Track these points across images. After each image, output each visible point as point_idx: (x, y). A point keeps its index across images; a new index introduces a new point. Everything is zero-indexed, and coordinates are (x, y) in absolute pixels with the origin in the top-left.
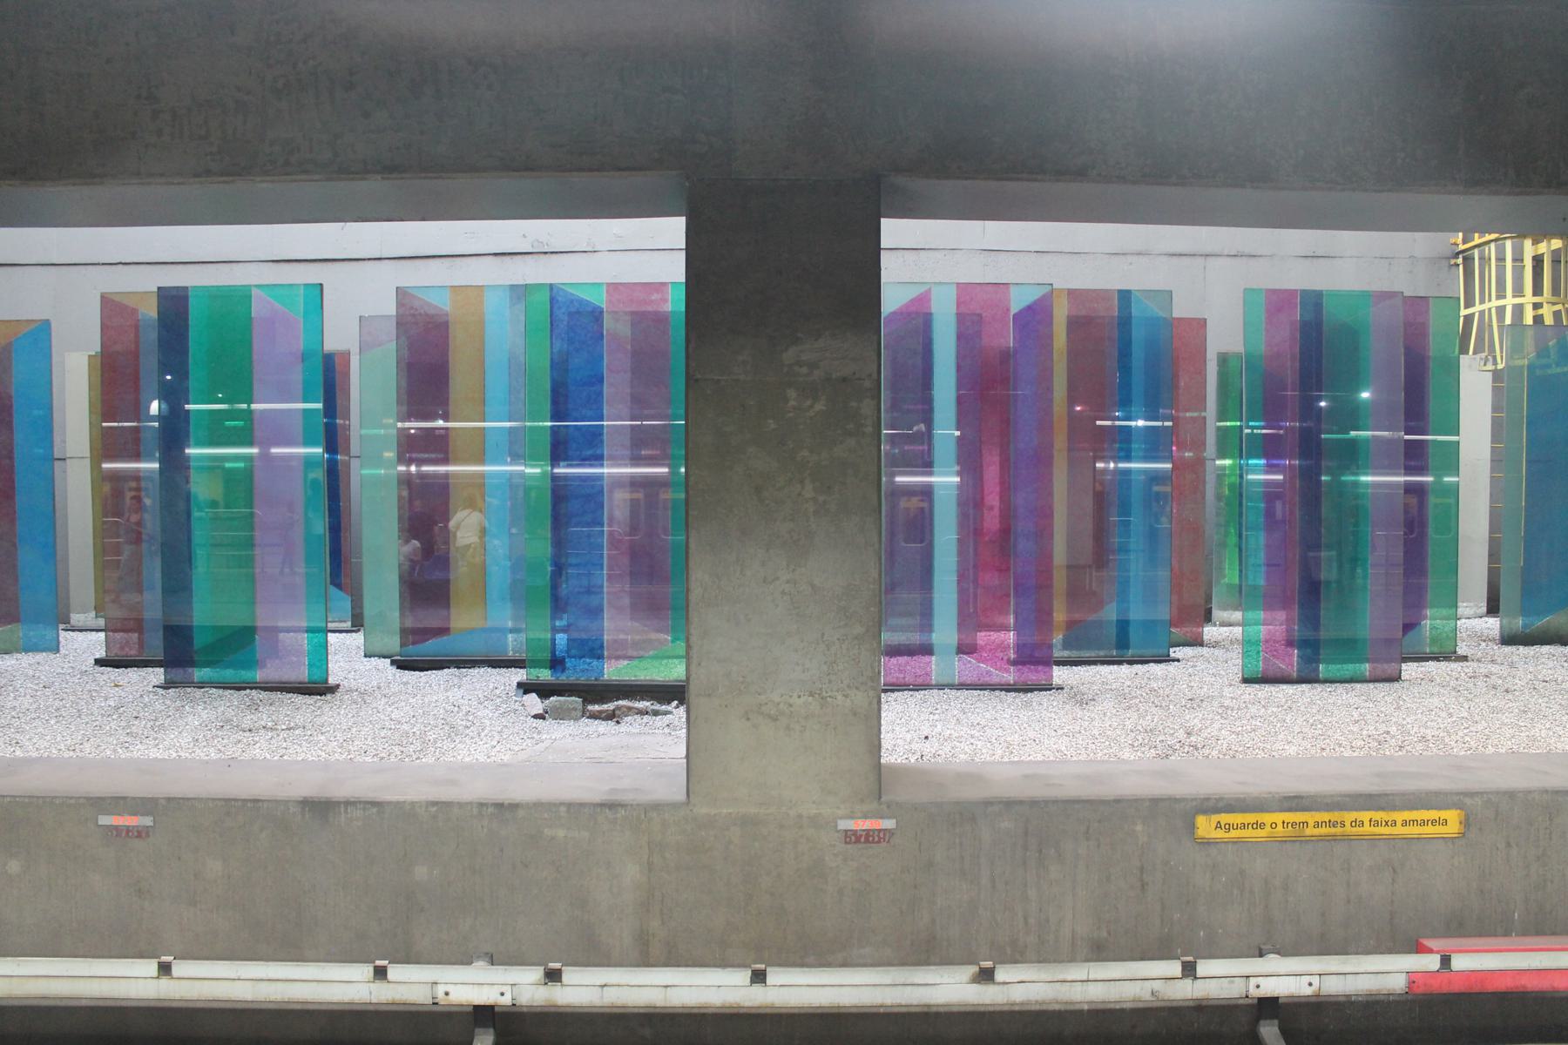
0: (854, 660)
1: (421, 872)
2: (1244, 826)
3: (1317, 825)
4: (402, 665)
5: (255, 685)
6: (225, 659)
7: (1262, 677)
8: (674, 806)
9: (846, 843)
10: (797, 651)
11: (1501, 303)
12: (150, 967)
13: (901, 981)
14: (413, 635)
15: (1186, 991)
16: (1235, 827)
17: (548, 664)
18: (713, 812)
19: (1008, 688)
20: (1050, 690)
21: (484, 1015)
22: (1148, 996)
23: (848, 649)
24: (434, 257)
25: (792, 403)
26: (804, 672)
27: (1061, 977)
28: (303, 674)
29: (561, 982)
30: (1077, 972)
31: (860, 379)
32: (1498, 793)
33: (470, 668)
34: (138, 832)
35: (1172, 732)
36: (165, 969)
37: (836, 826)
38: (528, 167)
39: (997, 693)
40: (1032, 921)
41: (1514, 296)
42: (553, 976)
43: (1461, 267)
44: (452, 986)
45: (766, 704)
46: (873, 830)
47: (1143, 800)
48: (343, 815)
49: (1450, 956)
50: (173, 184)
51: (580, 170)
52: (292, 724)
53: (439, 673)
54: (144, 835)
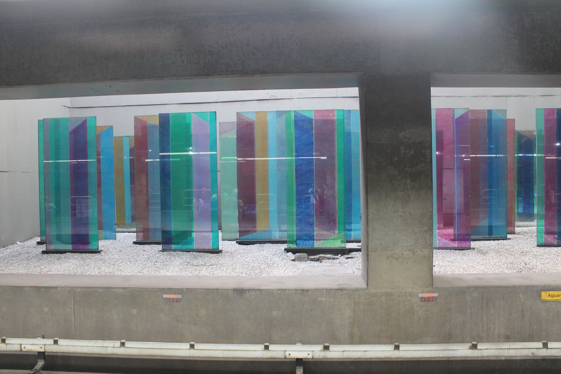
1: (275, 313)
4: (240, 243)
5: (192, 250)
6: (183, 241)
7: (544, 245)
8: (363, 289)
9: (421, 301)
10: (405, 236)
12: (187, 346)
14: (242, 233)
15: (544, 353)
16: (555, 296)
18: (376, 291)
19: (456, 249)
20: (470, 249)
21: (299, 362)
22: (531, 355)
23: (422, 235)
25: (402, 151)
26: (407, 243)
27: (500, 347)
28: (210, 246)
29: (329, 350)
31: (425, 143)
33: (264, 244)
34: (177, 300)
35: (519, 263)
36: (192, 346)
37: (418, 296)
38: (310, 71)
39: (452, 250)
42: (326, 348)
45: (394, 254)
46: (431, 297)
48: (248, 294)
50: (187, 79)
51: (328, 72)
52: (211, 264)
54: (178, 301)
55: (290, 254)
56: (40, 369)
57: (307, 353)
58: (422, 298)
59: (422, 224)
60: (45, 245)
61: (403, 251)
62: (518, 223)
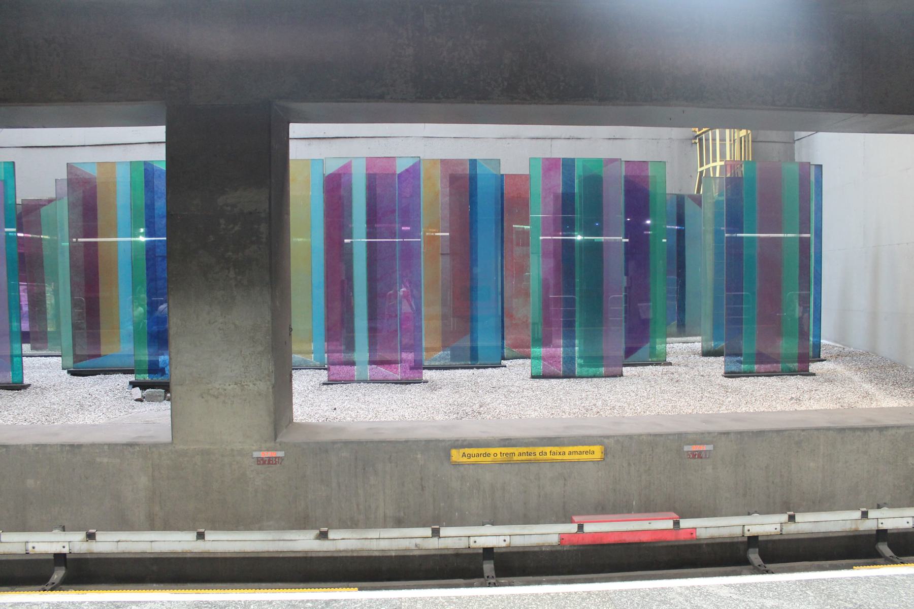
0: (258, 365)
1: (30, 483)
2: (478, 455)
3: (520, 454)
4: (74, 373)
8: (165, 445)
9: (258, 464)
10: (227, 360)
11: (714, 164)
13: (277, 538)
15: (434, 544)
17: (147, 372)
20: (420, 383)
22: (413, 547)
24: (105, 145)
27: (364, 537)
29: (95, 540)
30: (373, 534)
32: (623, 436)
37: (252, 455)
39: (389, 385)
40: (361, 507)
41: (720, 161)
43: (698, 144)
44: (37, 543)
45: (212, 389)
46: (273, 457)
47: (421, 441)
49: (583, 524)
53: (93, 377)
56: (59, 583)
57: (61, 544)
58: (259, 459)
59: (253, 341)
61: (225, 385)
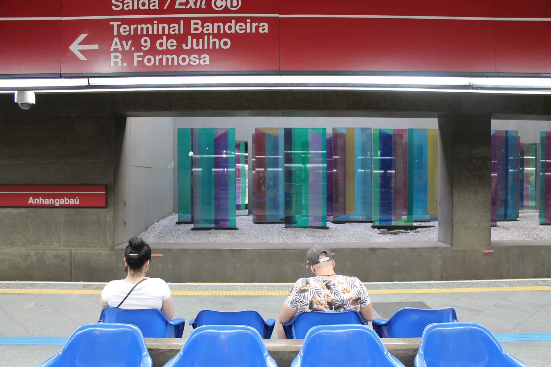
1: (395, 263)
9: (484, 255)
55: (376, 229)
60: (193, 224)
62: (322, 224)
